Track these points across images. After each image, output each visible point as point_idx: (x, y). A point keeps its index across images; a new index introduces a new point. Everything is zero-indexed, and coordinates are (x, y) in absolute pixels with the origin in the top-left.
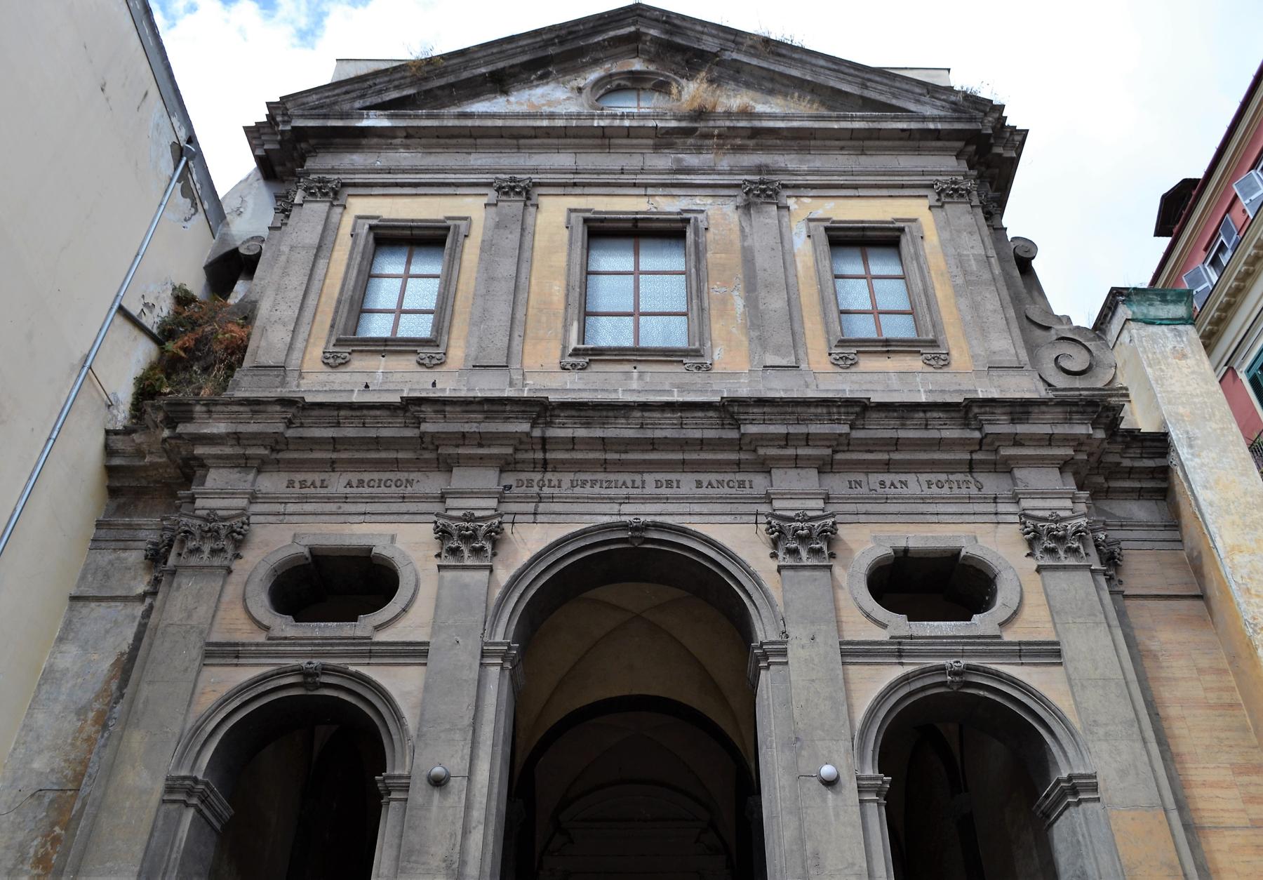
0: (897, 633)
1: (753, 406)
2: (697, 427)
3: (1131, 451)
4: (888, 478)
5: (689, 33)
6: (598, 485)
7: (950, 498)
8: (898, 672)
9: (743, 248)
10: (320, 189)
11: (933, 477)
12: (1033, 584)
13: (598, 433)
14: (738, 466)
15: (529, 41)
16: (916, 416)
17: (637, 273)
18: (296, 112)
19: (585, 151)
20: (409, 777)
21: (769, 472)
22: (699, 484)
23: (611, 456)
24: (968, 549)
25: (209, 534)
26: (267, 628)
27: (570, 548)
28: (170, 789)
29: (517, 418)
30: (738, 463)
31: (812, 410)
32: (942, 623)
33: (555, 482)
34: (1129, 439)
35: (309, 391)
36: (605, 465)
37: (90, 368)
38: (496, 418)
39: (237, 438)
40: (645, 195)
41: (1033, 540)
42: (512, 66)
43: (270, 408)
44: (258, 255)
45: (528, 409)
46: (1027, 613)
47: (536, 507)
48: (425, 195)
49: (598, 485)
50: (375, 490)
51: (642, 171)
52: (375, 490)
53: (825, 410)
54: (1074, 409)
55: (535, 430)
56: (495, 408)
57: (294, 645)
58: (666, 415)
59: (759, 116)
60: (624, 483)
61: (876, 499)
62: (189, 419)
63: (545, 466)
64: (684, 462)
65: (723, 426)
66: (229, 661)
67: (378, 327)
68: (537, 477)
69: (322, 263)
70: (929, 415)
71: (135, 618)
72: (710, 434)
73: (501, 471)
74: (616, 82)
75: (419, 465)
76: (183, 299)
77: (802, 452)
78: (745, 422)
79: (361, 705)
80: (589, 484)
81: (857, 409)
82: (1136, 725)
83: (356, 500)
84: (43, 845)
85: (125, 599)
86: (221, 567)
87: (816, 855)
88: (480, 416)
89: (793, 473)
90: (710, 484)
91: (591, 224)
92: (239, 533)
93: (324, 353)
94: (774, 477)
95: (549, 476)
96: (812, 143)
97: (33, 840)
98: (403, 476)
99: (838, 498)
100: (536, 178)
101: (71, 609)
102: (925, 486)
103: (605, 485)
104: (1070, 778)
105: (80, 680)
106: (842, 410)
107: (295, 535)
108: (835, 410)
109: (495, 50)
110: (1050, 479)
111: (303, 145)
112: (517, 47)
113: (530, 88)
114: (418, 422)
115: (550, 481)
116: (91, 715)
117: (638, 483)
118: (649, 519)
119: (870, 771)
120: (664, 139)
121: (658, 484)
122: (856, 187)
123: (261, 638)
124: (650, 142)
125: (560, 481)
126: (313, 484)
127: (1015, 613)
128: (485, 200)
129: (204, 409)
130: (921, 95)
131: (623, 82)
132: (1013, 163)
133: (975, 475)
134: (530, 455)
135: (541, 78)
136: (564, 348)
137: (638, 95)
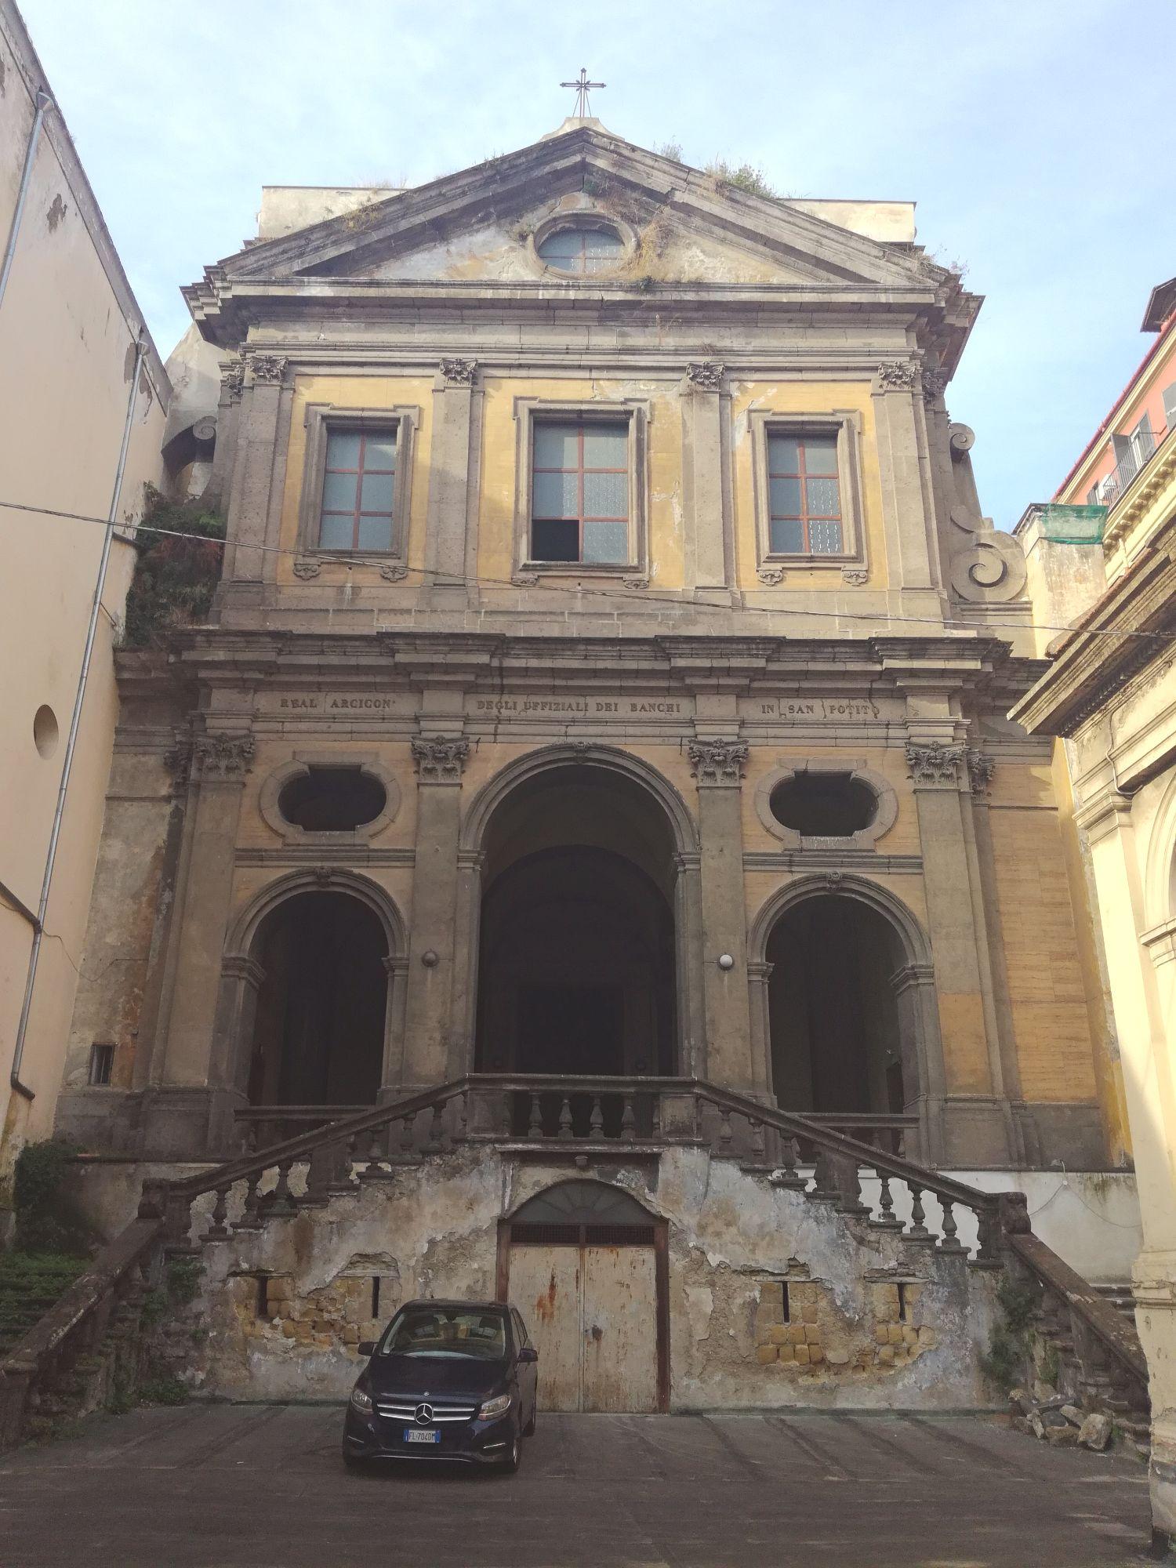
0: (790, 847)
1: (684, 643)
2: (634, 658)
3: (1020, 674)
4: (797, 703)
5: (638, 166)
6: (548, 707)
7: (848, 724)
8: (788, 879)
9: (684, 445)
10: (269, 371)
11: (835, 703)
12: (908, 803)
13: (547, 663)
14: (668, 691)
15: (470, 180)
16: (825, 650)
17: (582, 471)
18: (235, 278)
19: (529, 323)
20: (408, 959)
21: (695, 697)
22: (634, 708)
23: (558, 682)
24: (860, 773)
25: (223, 754)
26: (283, 836)
27: (525, 767)
28: (225, 967)
29: (478, 650)
30: (668, 689)
31: (734, 646)
32: (828, 838)
33: (510, 704)
34: (1017, 666)
35: (289, 610)
36: (554, 690)
37: (101, 603)
38: (460, 650)
39: (235, 665)
40: (590, 379)
41: (915, 763)
42: (453, 211)
43: (262, 639)
44: (213, 440)
45: (487, 643)
46: (900, 829)
47: (496, 728)
48: (373, 376)
49: (548, 707)
50: (358, 711)
51: (587, 351)
52: (358, 711)
53: (745, 647)
54: (968, 646)
55: (493, 660)
56: (459, 642)
57: (307, 851)
58: (606, 649)
59: (708, 287)
60: (570, 706)
61: (784, 724)
62: (192, 647)
63: (502, 689)
64: (621, 688)
65: (656, 658)
66: (254, 863)
67: (340, 536)
68: (495, 698)
69: (280, 459)
70: (837, 650)
71: (164, 816)
72: (645, 665)
73: (465, 693)
74: (560, 226)
75: (394, 687)
76: (151, 494)
77: (723, 681)
78: (675, 655)
79: (364, 900)
80: (540, 707)
81: (773, 646)
82: (972, 927)
83: (345, 718)
84: (128, 1002)
85: (152, 799)
86: (238, 782)
87: (713, 1021)
88: (447, 648)
89: (715, 699)
90: (643, 707)
91: (537, 415)
92: (249, 752)
93: (295, 565)
94: (698, 702)
95: (506, 698)
96: (760, 315)
97: (119, 998)
98: (381, 696)
99: (752, 723)
100: (482, 358)
101: (108, 806)
102: (828, 711)
103: (553, 707)
104: (913, 968)
105: (128, 871)
106: (760, 646)
107: (294, 752)
108: (754, 646)
109: (433, 193)
110: (940, 709)
111: (245, 313)
112: (457, 188)
113: (471, 233)
114: (393, 653)
115: (506, 703)
116: (144, 899)
117: (582, 706)
118: (592, 741)
119: (759, 959)
120: (607, 314)
121: (599, 707)
122: (800, 370)
123: (278, 845)
124: (595, 314)
125: (515, 703)
126: (304, 703)
127: (890, 830)
128: (431, 384)
129: (203, 638)
130: (876, 257)
131: (567, 225)
132: (965, 332)
133: (873, 701)
134: (489, 681)
135: (482, 220)
136: (516, 561)
137: (584, 239)
